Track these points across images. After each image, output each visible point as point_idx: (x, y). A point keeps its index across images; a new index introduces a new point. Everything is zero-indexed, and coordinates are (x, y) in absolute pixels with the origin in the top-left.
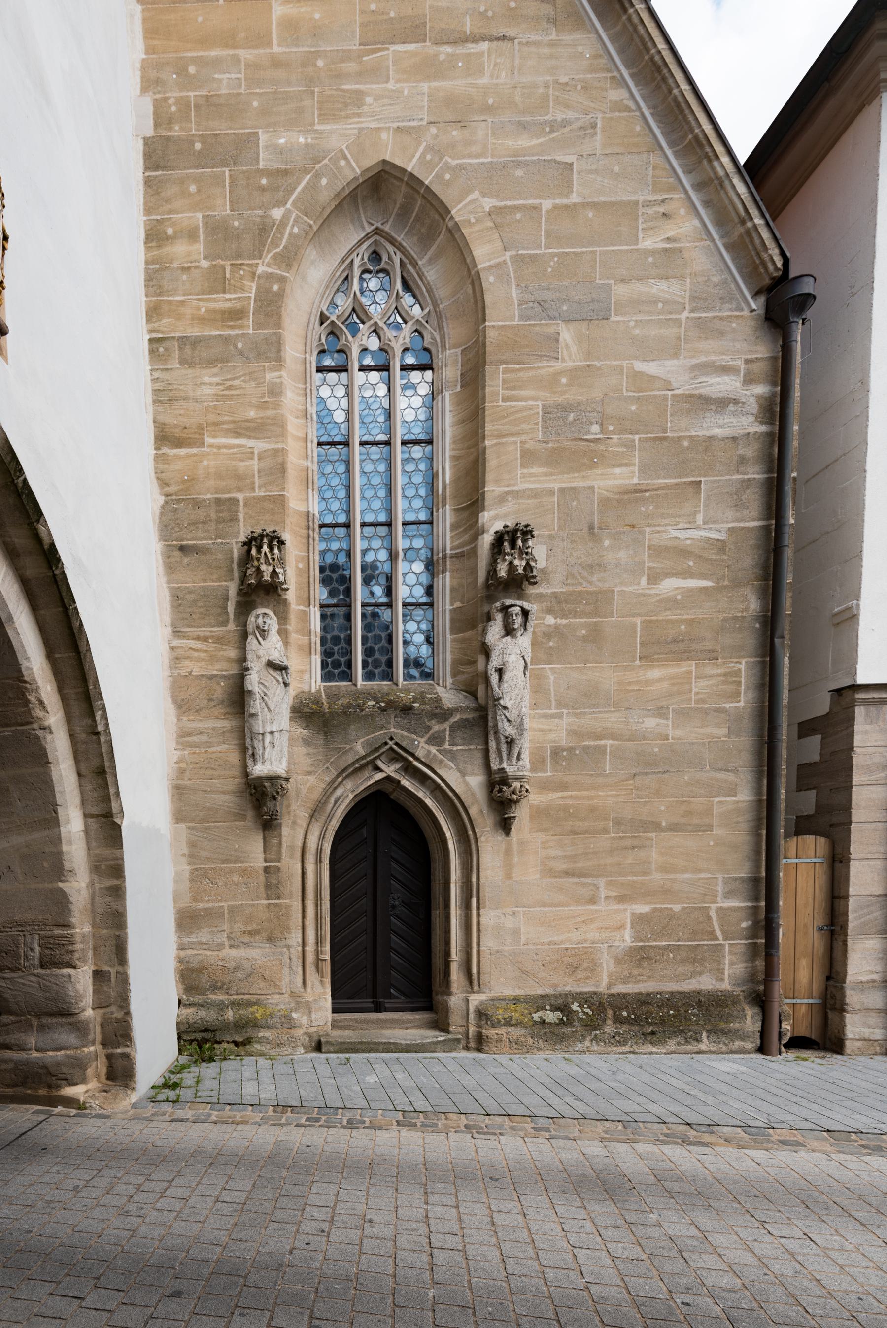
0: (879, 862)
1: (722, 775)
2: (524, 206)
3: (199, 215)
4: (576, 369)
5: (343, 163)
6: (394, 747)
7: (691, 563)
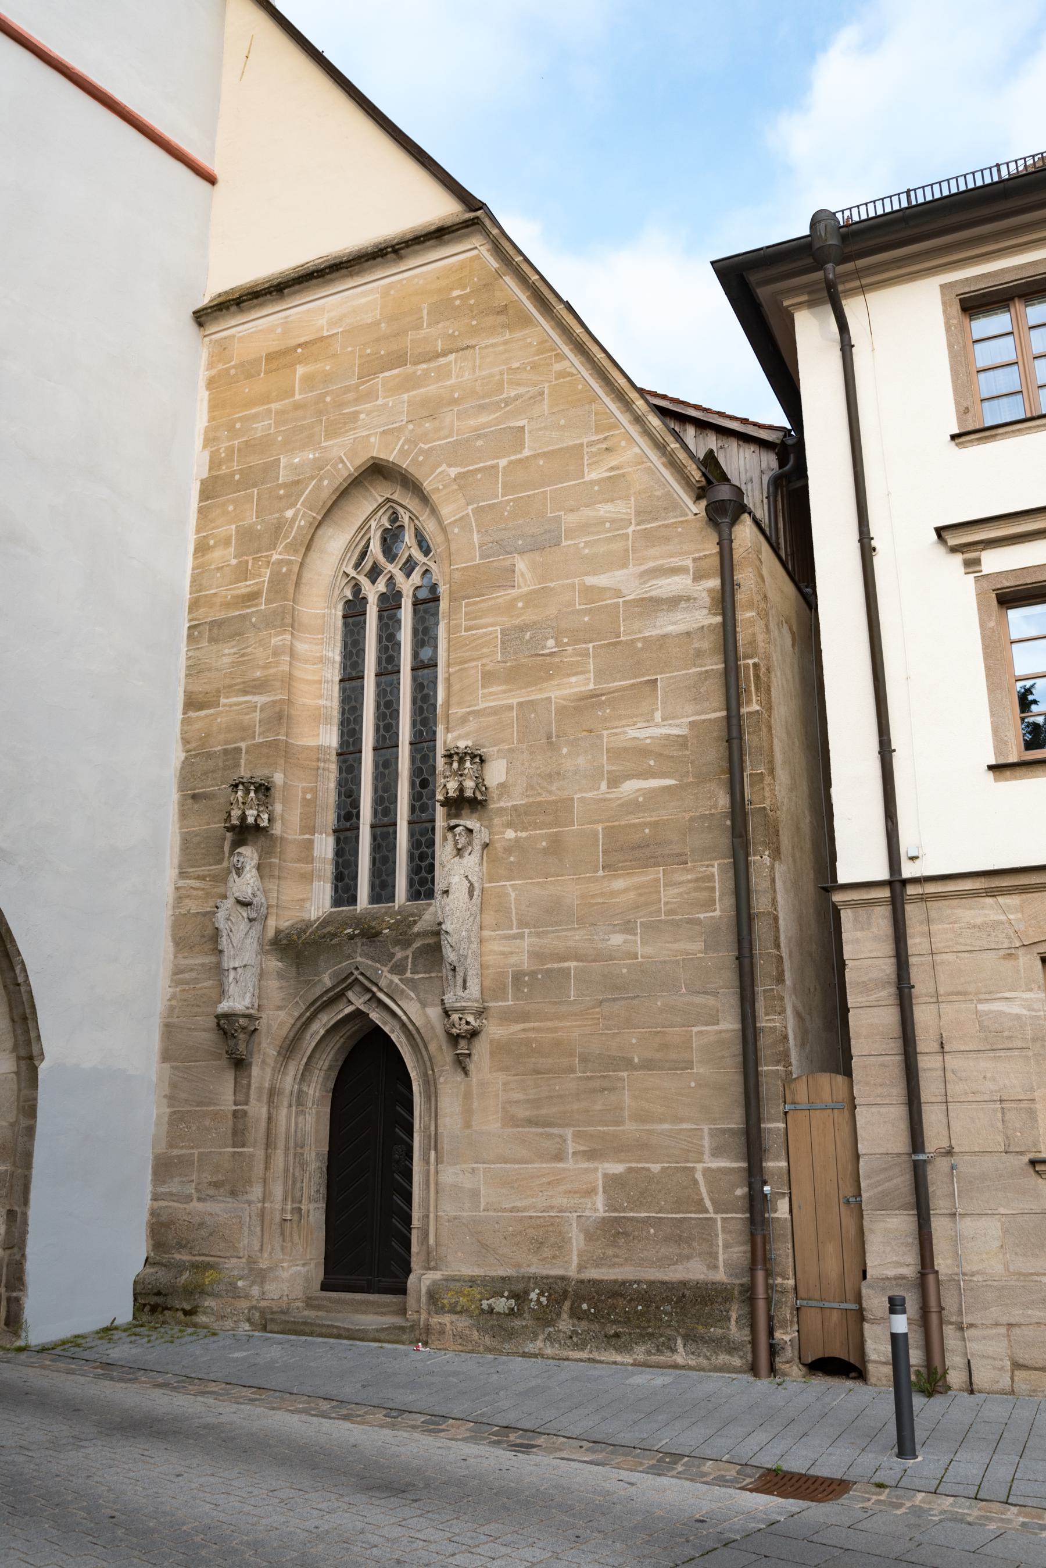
0: (892, 1109)
1: (699, 1000)
2: (484, 467)
3: (233, 527)
4: (531, 593)
5: (340, 466)
6: (360, 977)
7: (652, 763)
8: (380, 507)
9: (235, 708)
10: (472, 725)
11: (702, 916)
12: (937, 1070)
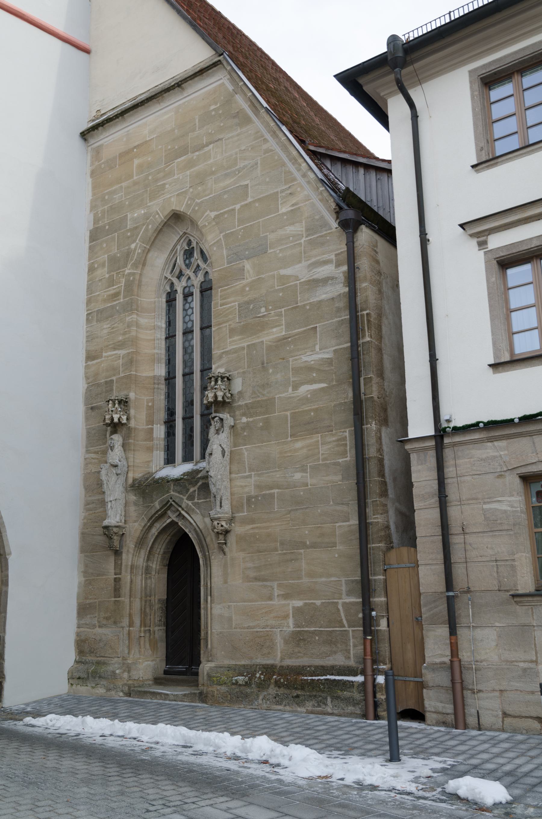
1: (339, 508)
2: (228, 211)
3: (106, 256)
4: (254, 281)
5: (157, 216)
6: (173, 503)
7: (314, 375)
8: (181, 237)
9: (110, 358)
10: (224, 360)
11: (340, 460)
12: (461, 543)
